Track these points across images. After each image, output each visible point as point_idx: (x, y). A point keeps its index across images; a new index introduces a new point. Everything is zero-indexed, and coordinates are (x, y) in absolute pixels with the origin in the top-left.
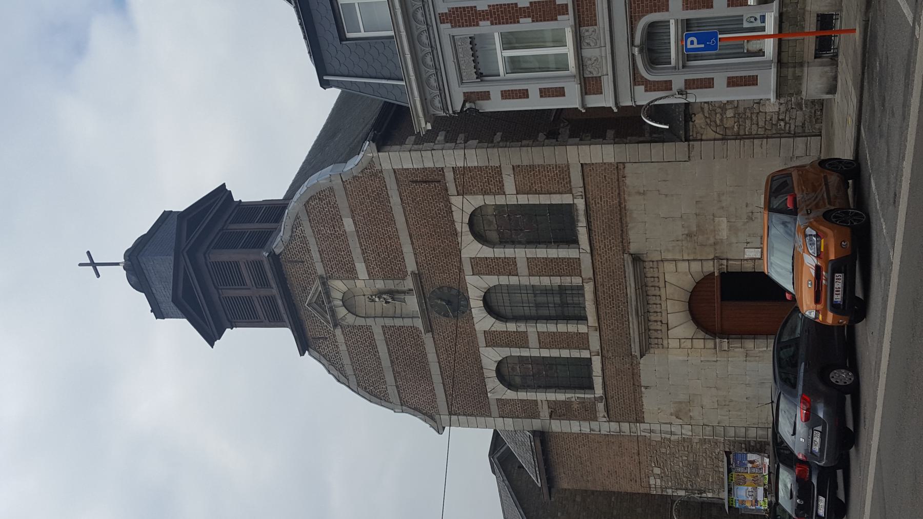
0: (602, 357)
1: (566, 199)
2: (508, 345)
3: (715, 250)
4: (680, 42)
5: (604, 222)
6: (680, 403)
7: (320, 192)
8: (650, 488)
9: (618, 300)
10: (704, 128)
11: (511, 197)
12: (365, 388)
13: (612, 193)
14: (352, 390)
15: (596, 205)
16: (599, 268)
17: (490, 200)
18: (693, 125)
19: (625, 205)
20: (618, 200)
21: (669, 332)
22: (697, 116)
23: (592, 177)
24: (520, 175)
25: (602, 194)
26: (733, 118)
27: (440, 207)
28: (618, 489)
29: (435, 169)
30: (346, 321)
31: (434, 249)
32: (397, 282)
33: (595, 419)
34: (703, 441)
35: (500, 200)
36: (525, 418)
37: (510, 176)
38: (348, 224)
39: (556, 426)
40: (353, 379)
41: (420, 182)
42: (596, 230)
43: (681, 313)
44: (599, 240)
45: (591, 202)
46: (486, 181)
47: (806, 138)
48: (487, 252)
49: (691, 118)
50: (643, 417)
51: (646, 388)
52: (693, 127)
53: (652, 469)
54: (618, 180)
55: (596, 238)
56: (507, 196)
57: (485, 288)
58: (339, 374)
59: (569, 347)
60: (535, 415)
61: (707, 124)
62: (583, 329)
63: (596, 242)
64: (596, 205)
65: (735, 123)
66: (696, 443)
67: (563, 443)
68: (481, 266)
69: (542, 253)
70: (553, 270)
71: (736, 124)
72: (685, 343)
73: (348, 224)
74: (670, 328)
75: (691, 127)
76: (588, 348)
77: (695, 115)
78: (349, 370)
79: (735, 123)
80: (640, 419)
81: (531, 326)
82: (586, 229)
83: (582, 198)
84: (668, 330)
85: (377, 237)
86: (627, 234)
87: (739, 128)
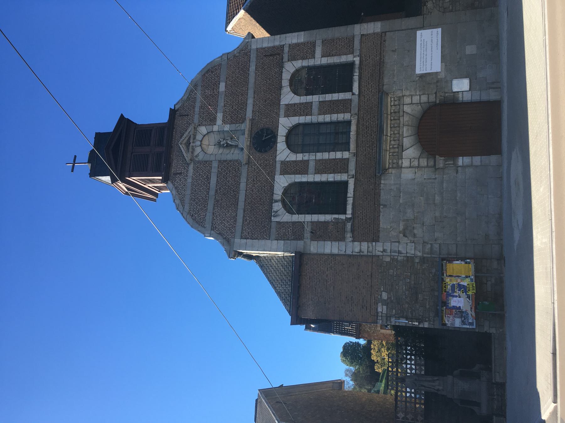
0: (355, 179)
1: (349, 58)
2: (295, 173)
3: (437, 86)
4: (422, 59)
5: (370, 72)
6: (407, 220)
7: (213, 67)
8: (377, 316)
9: (372, 130)
10: (433, 9)
11: (319, 60)
12: (192, 216)
13: (377, 52)
14: (183, 217)
15: (366, 61)
16: (362, 106)
17: (305, 63)
18: (426, 8)
19: (383, 60)
20: (379, 57)
21: (403, 153)
22: (429, 2)
23: (366, 43)
24: (325, 45)
25: (370, 54)
26: (449, 3)
27: (276, 71)
28: (351, 319)
29: (279, 47)
30: (198, 157)
31: (265, 101)
32: (237, 125)
33: (343, 239)
34: (423, 260)
35: (311, 62)
36: (293, 240)
37: (320, 46)
38: (222, 87)
39: (315, 247)
40: (187, 207)
41: (269, 55)
42: (364, 78)
43: (412, 136)
44: (365, 85)
45: (363, 59)
46: (305, 52)
47: (277, 162)
48: (297, 99)
49: (425, 4)
50: (379, 236)
51: (385, 206)
52: (426, 9)
53: (380, 294)
54: (381, 43)
55: (363, 84)
56: (320, 59)
57: (289, 127)
58: (180, 204)
59: (334, 172)
60: (299, 237)
61: (434, 7)
62: (346, 155)
63: (363, 87)
64: (366, 61)
65: (450, 5)
66: (417, 263)
67: (316, 266)
68: (292, 110)
69: (329, 97)
70: (333, 110)
71: (450, 6)
72: (414, 162)
73: (222, 87)
74: (404, 149)
75: (425, 9)
76: (347, 172)
77: (428, 2)
78: (187, 200)
79: (450, 5)
80: (376, 239)
81: (312, 155)
82: (358, 77)
83: (359, 57)
84: (403, 151)
85: (235, 95)
86: (382, 79)
87: (452, 8)
